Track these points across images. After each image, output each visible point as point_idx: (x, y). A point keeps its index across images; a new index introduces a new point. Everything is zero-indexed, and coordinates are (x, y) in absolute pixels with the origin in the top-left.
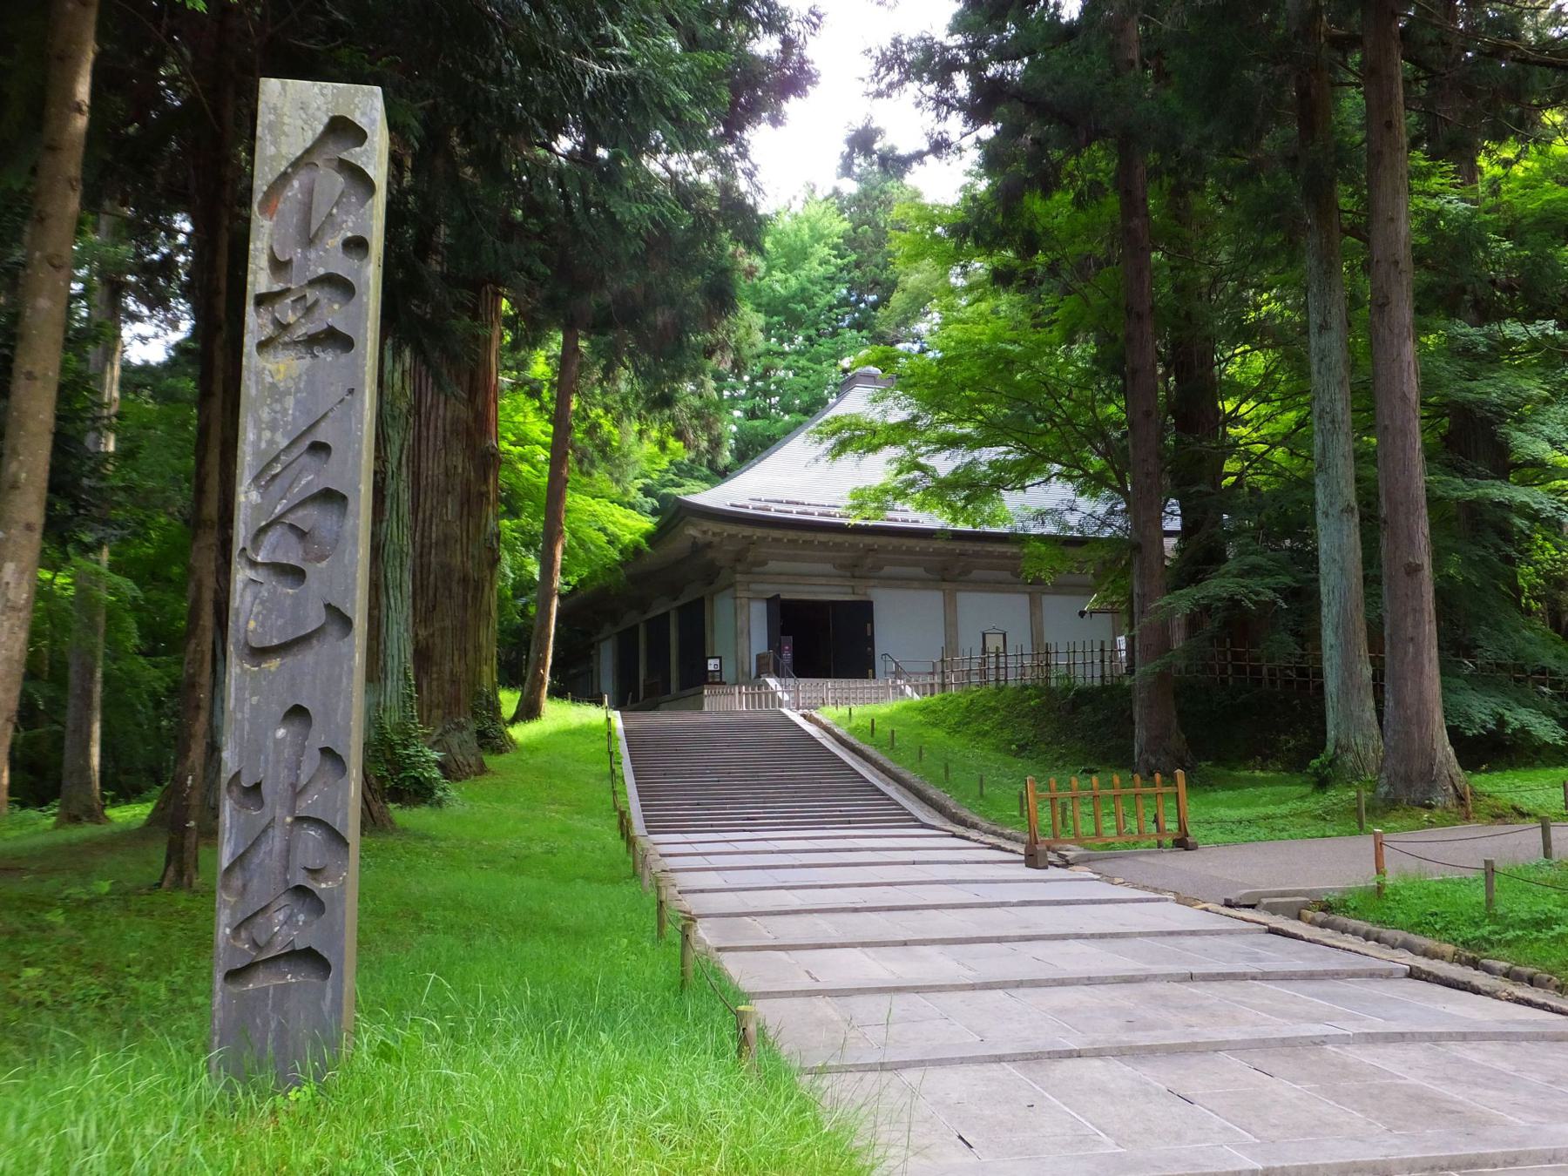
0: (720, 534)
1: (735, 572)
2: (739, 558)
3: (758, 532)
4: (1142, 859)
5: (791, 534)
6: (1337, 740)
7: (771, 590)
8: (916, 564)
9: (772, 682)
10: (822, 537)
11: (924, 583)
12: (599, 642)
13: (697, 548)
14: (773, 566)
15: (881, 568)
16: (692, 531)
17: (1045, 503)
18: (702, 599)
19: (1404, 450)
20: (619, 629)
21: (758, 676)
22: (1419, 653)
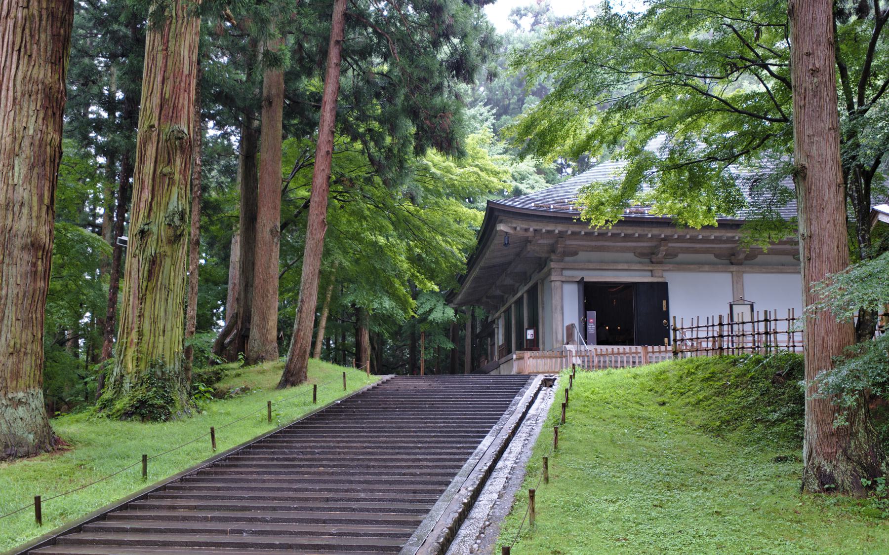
2: (552, 250)
7: (578, 275)
11: (713, 267)
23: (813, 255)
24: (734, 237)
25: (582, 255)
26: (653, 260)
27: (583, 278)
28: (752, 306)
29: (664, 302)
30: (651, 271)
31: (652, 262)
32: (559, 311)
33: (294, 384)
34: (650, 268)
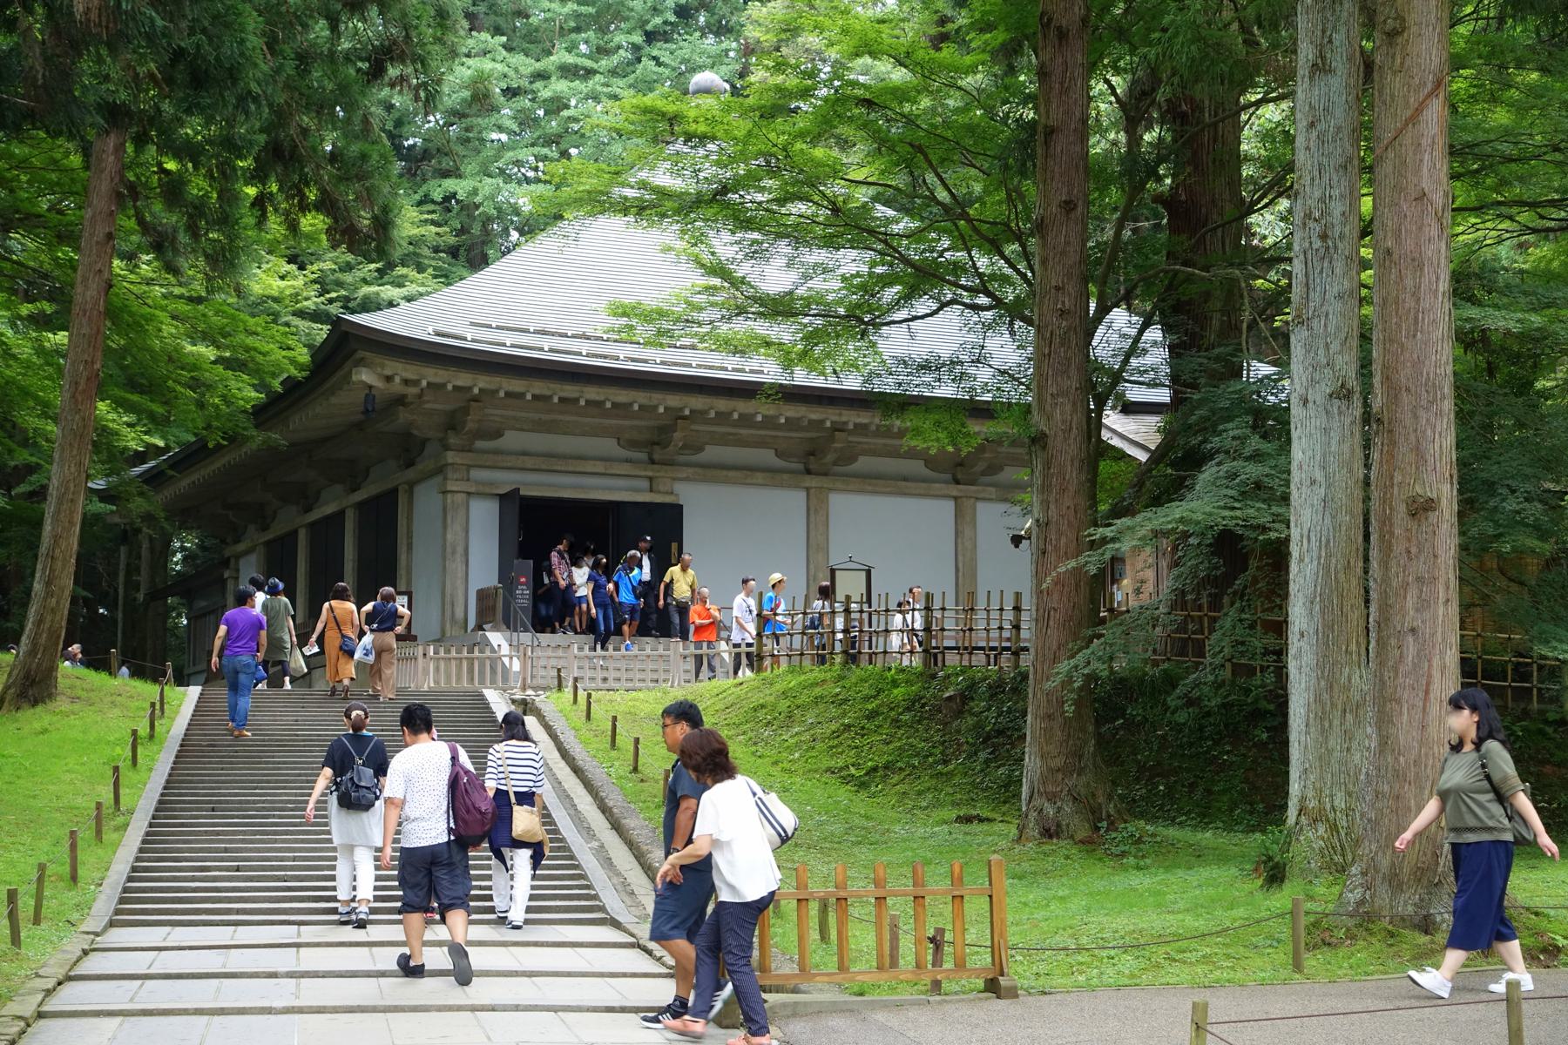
0: (416, 383)
1: (447, 448)
2: (453, 423)
3: (481, 382)
4: (880, 1016)
5: (539, 387)
6: (1303, 799)
7: (506, 480)
8: (761, 444)
9: (496, 638)
10: (592, 393)
11: (772, 476)
12: (238, 557)
13: (376, 408)
14: (512, 440)
15: (701, 449)
16: (365, 376)
17: (947, 344)
18: (394, 492)
19: (1416, 295)
20: (269, 536)
21: (480, 627)
22: (1423, 656)
23: (1049, 548)
24: (822, 422)
25: (511, 440)
26: (656, 457)
27: (518, 490)
28: (869, 573)
29: (674, 546)
30: (651, 479)
31: (653, 462)
32: (459, 557)
33: (35, 703)
34: (650, 474)
